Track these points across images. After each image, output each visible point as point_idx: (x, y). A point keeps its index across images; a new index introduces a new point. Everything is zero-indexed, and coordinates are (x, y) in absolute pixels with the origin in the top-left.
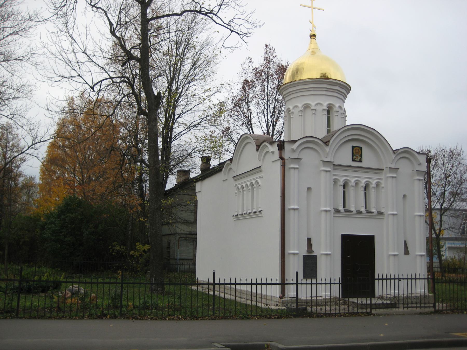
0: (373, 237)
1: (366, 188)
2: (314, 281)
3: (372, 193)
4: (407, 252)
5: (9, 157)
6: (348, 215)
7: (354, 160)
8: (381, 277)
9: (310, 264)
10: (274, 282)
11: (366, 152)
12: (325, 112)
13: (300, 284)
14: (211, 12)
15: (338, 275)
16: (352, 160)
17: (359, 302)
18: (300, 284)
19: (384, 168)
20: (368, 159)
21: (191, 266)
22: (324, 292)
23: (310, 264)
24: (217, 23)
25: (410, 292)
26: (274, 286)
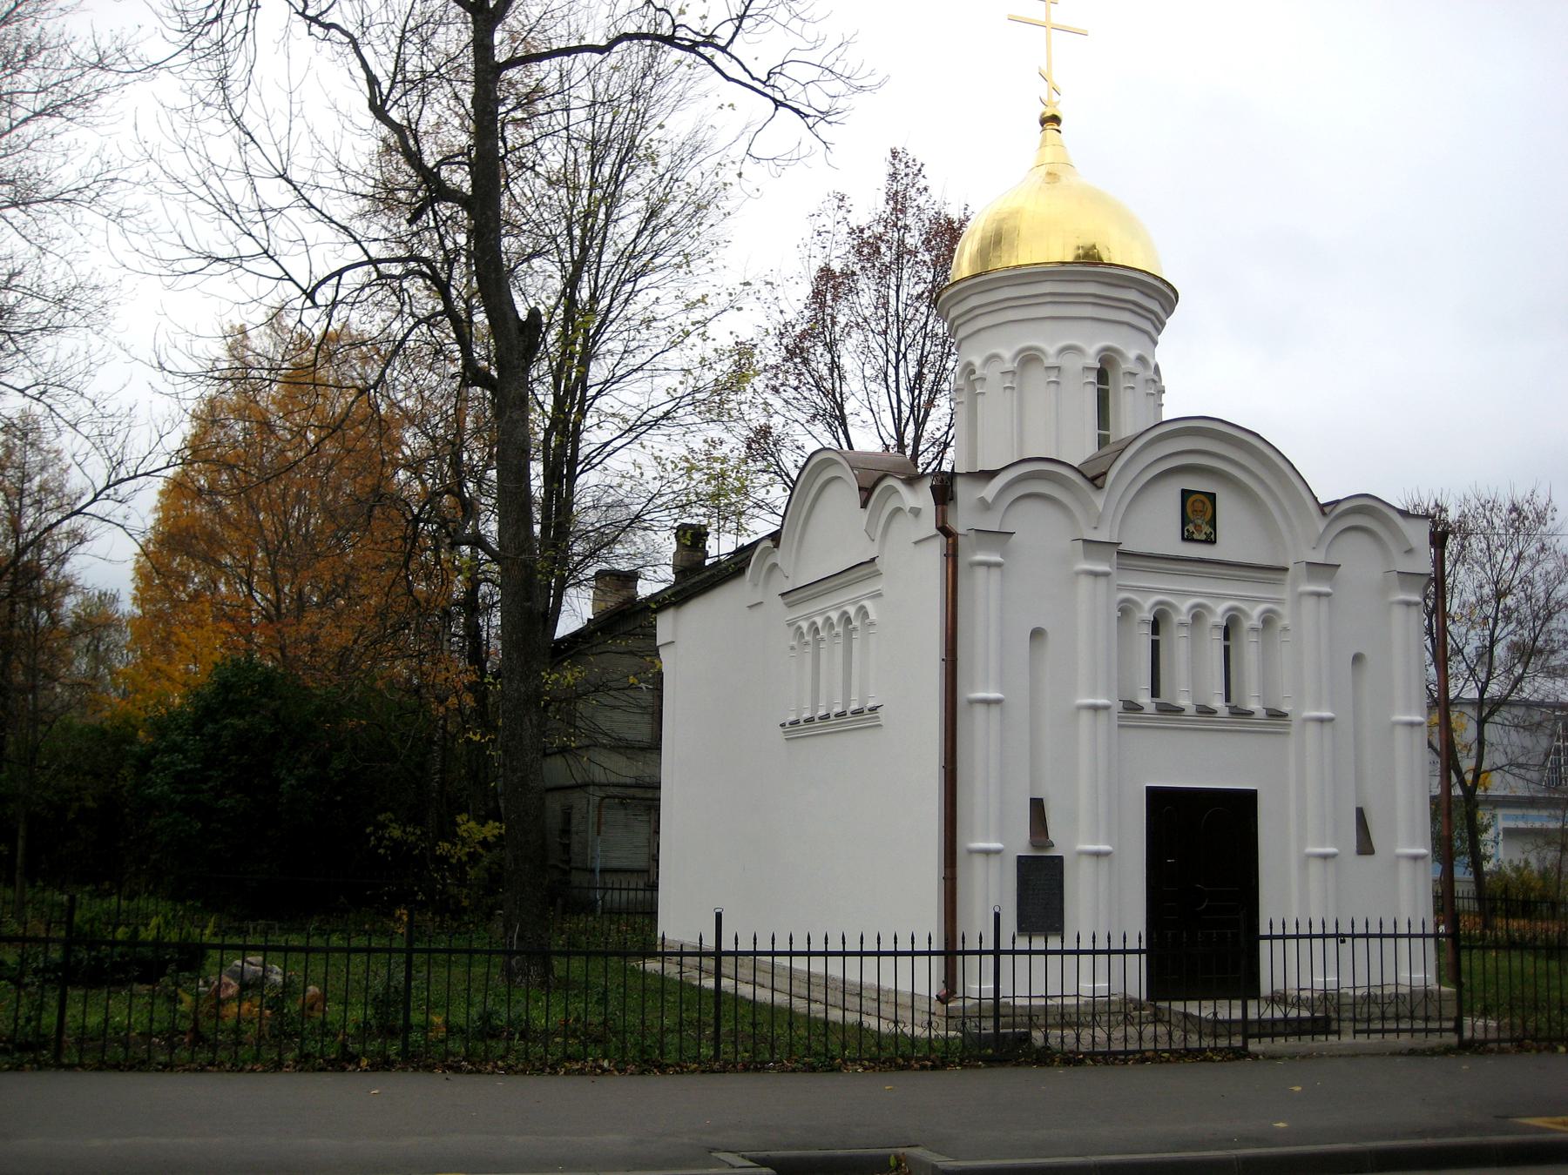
1: (1229, 630)
2: (1054, 943)
3: (1249, 649)
4: (1365, 846)
7: (1187, 538)
8: (1278, 931)
9: (1041, 888)
10: (921, 945)
11: (1228, 510)
12: (1093, 378)
14: (709, 41)
15: (1134, 924)
16: (1183, 539)
17: (1207, 1013)
19: (1290, 565)
20: (1237, 535)
22: (1087, 982)
23: (1041, 888)
25: (1376, 980)
26: (921, 962)
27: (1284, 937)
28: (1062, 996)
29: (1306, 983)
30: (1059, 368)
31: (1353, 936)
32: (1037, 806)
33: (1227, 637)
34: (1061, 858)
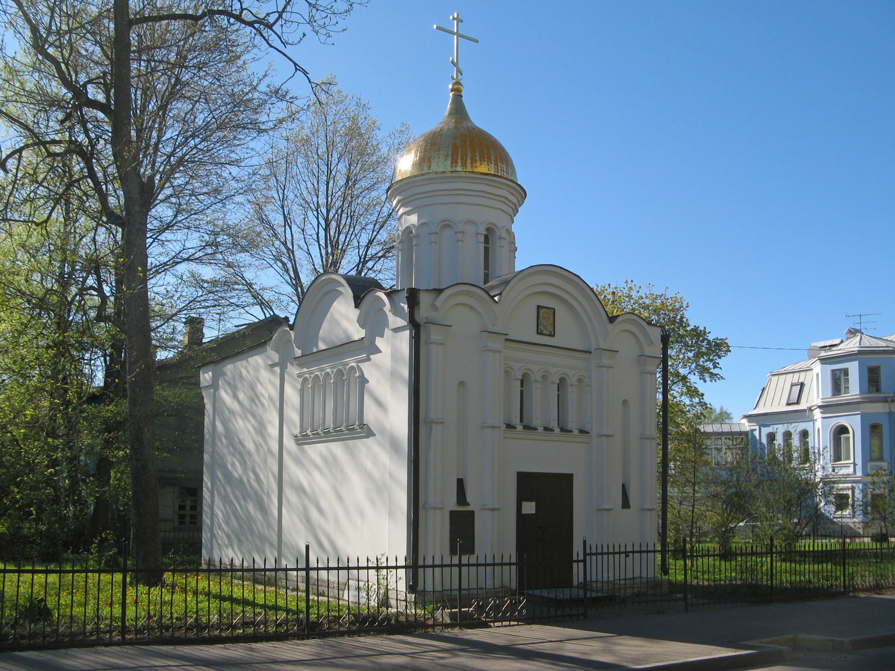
0: (572, 475)
1: (562, 384)
2: (473, 560)
3: (572, 394)
4: (626, 504)
5: (122, 211)
6: (529, 434)
7: (539, 332)
8: (594, 551)
9: (462, 527)
10: (506, 560)
11: (563, 318)
12: (482, 239)
13: (465, 565)
14: (260, 21)
15: (510, 550)
16: (538, 333)
17: (552, 596)
18: (465, 565)
19: (592, 350)
20: (566, 332)
21: (172, 534)
22: (487, 579)
23: (462, 527)
24: (271, 46)
25: (617, 577)
26: (506, 568)
27: (647, 552)
28: (451, 590)
29: (600, 579)
30: (463, 232)
31: (633, 552)
32: (460, 483)
33: (522, 386)
34: (473, 512)
